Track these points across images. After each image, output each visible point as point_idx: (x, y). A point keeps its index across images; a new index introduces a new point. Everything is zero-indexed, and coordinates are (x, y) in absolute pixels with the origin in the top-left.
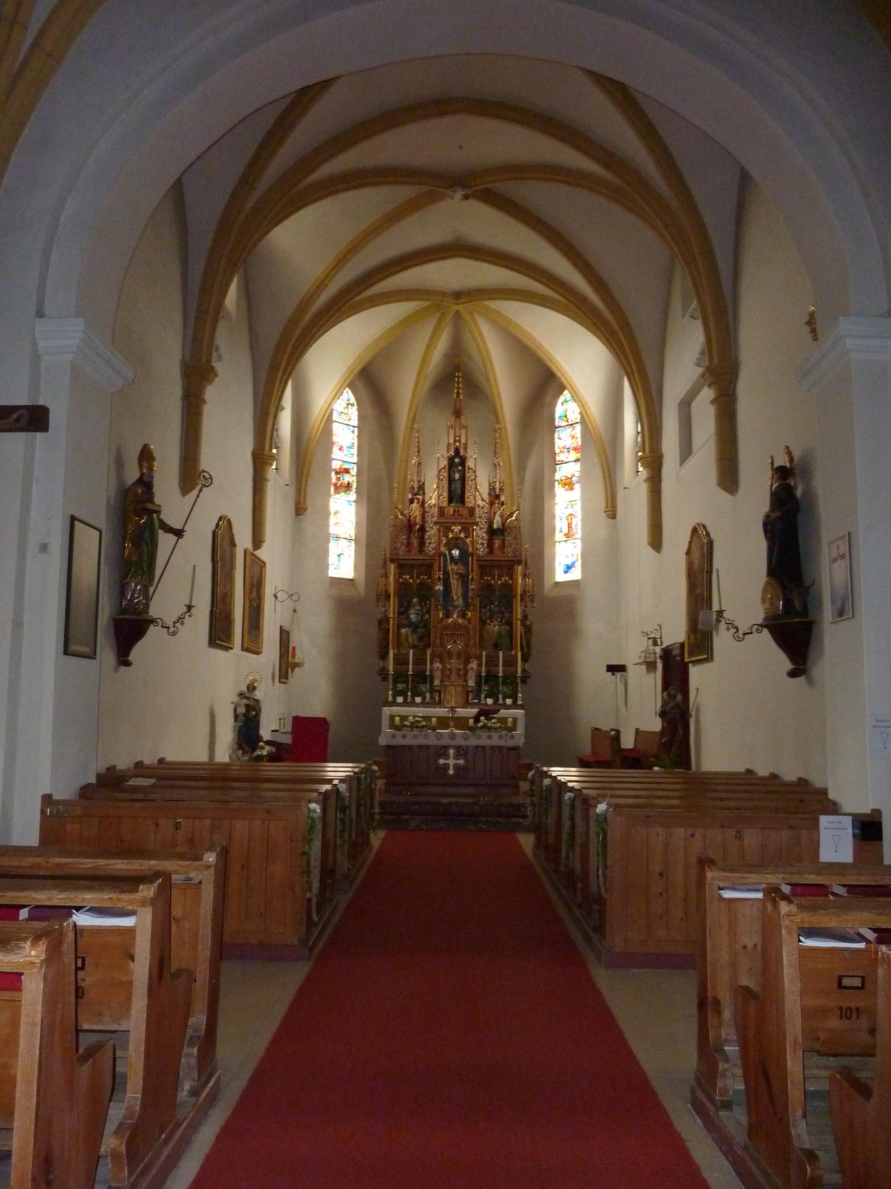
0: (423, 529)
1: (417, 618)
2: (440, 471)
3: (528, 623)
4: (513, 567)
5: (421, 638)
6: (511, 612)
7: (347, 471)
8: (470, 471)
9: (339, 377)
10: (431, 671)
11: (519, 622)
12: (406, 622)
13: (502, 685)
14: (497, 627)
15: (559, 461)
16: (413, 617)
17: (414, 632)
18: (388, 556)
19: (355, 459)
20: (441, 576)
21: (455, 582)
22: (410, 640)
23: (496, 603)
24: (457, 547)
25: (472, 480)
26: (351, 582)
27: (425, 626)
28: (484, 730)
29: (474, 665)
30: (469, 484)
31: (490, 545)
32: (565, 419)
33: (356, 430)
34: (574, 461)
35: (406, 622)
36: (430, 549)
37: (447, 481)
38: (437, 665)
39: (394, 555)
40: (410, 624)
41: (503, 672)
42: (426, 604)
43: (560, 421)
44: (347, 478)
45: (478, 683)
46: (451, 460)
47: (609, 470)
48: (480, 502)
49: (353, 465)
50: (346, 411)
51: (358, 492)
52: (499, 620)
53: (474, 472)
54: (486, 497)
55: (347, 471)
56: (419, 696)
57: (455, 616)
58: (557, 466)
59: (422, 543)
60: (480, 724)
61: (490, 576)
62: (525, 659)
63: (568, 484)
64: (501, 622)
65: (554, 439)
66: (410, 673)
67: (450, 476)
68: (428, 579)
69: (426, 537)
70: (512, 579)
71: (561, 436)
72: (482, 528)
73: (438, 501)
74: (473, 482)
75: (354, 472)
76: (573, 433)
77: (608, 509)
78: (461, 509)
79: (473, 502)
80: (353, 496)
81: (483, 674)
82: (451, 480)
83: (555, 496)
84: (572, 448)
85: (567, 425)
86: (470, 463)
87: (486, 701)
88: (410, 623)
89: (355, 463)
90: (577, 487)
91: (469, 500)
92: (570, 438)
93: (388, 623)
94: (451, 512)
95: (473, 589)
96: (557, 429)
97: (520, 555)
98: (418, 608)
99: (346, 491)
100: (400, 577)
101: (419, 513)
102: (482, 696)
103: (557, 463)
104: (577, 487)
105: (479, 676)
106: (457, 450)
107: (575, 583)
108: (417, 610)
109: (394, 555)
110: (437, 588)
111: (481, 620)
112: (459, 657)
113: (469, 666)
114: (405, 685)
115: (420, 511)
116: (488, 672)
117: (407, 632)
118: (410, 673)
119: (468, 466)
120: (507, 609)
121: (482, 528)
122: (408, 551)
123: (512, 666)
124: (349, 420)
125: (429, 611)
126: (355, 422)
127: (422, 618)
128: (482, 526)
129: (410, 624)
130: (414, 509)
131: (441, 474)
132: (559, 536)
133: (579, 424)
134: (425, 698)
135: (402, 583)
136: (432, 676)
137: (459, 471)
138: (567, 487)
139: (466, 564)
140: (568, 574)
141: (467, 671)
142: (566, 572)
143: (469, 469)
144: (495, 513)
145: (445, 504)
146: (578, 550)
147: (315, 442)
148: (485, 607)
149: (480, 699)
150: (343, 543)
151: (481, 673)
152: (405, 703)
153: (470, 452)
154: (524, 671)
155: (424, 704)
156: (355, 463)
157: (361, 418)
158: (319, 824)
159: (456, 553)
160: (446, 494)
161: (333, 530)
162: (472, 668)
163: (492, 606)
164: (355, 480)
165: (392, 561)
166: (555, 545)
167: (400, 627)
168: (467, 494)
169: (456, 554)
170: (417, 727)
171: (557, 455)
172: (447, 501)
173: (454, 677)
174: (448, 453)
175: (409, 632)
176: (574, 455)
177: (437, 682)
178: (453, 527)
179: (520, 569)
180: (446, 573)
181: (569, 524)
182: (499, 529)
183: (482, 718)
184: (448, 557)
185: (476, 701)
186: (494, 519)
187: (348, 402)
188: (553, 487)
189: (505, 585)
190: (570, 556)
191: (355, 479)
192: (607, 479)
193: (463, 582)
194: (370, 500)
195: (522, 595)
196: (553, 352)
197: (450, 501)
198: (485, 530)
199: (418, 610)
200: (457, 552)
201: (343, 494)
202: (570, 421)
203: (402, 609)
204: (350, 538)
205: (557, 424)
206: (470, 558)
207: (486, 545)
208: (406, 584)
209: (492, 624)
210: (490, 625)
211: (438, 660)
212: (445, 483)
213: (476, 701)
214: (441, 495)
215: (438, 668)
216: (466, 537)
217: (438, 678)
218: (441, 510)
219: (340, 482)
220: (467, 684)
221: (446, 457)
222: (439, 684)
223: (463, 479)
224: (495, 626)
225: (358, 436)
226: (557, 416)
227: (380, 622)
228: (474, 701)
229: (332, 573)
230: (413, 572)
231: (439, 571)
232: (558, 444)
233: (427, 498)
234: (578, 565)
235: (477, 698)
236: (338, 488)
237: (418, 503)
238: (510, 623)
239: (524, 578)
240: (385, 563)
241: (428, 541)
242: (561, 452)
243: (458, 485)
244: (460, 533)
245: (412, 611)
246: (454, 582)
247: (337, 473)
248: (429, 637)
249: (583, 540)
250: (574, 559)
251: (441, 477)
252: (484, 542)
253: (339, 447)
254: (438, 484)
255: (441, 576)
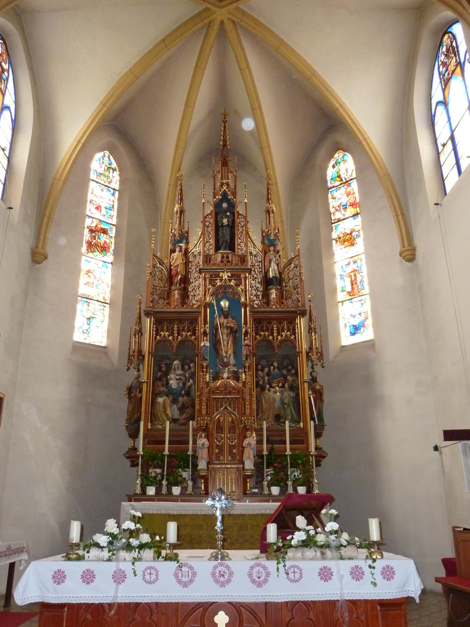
0: (185, 280)
1: (178, 384)
2: (205, 217)
3: (318, 387)
4: (295, 320)
5: (182, 409)
6: (296, 374)
7: (104, 231)
8: (240, 217)
9: (91, 113)
10: (195, 451)
11: (306, 385)
12: (163, 389)
13: (291, 467)
14: (278, 394)
15: (335, 220)
16: (173, 383)
17: (174, 401)
18: (143, 308)
19: (114, 221)
20: (208, 330)
21: (225, 337)
22: (169, 412)
23: (276, 364)
24: (225, 297)
25: (242, 227)
26: (104, 349)
27: (188, 394)
28: (310, 553)
29: (251, 440)
30: (239, 230)
31: (266, 295)
32: (338, 179)
33: (117, 194)
34: (352, 217)
35: (163, 389)
36: (194, 302)
37: (214, 227)
38: (203, 441)
39: (149, 307)
40: (170, 392)
41: (291, 450)
42: (190, 368)
43: (333, 182)
44: (103, 238)
45: (259, 466)
46: (217, 205)
47: (400, 204)
48: (252, 249)
49: (112, 226)
50: (107, 174)
51: (115, 253)
52: (280, 385)
53: (245, 217)
54: (259, 245)
55: (104, 231)
56: (177, 485)
57: (225, 375)
58: (333, 225)
59: (185, 295)
60: (299, 536)
61: (267, 330)
62: (318, 435)
63: (347, 240)
64: (283, 386)
65: (327, 199)
66: (166, 452)
67: (216, 222)
68: (191, 336)
69: (190, 290)
70: (294, 333)
71: (335, 196)
72: (256, 278)
73: (204, 249)
74: (244, 229)
75: (113, 233)
76: (349, 189)
77: (404, 249)
78: (230, 256)
79: (244, 249)
80: (109, 257)
81: (265, 453)
82: (218, 227)
83: (333, 254)
84: (348, 205)
85: (341, 184)
86: (240, 209)
87: (270, 490)
88: (169, 391)
89: (113, 225)
90: (360, 242)
91: (239, 247)
92: (345, 195)
93: (141, 391)
94: (219, 259)
95: (247, 345)
96: (330, 190)
97: (303, 305)
98: (180, 372)
99: (102, 251)
100: (157, 334)
101: (181, 261)
102: (265, 483)
103: (333, 222)
104: (360, 242)
105: (259, 455)
106: (225, 195)
107: (369, 345)
108: (177, 375)
109: (149, 307)
110: (202, 344)
111: (258, 385)
112: (232, 429)
113: (246, 442)
114: (159, 471)
115: (183, 260)
116: (271, 451)
117: (164, 401)
118: (166, 452)
119: (238, 212)
120: (289, 371)
121: (256, 278)
122: (168, 303)
123: (302, 442)
124: (109, 183)
125: (193, 376)
126: (116, 185)
127: (184, 384)
128: (255, 276)
129: (170, 392)
130: (175, 258)
131: (207, 220)
132: (341, 296)
133: (355, 180)
134: (187, 488)
135: (160, 341)
136: (195, 457)
137: (227, 217)
138: (346, 243)
139: (237, 318)
140: (356, 335)
141: (244, 448)
142: (353, 334)
143: (239, 214)
144: (270, 261)
145: (212, 252)
146: (368, 306)
147: (61, 183)
148: (262, 370)
149: (262, 488)
150: (95, 305)
151: (262, 451)
152: (159, 496)
153: (239, 197)
154: (317, 448)
155: (184, 497)
156: (113, 225)
157: (122, 182)
158: (226, 521)
159: (224, 304)
160: (212, 241)
161: (82, 290)
162: (249, 444)
163: (272, 368)
164: (113, 242)
165: (148, 314)
166: (337, 305)
167: (155, 395)
168: (237, 241)
169: (225, 305)
170: (129, 547)
171: (332, 214)
172: (213, 249)
173: (226, 457)
174: (214, 197)
175: (168, 402)
176: (351, 211)
177: (202, 465)
178: (221, 274)
179: (302, 323)
180: (215, 329)
181: (352, 282)
182: (274, 276)
183: (301, 521)
184: (216, 308)
185: (256, 490)
186: (270, 267)
187: (110, 166)
188: (331, 246)
189: (286, 340)
190: (357, 316)
191: (113, 240)
192: (400, 217)
193: (234, 338)
194: (128, 260)
195: (307, 353)
196: (328, 81)
197: (217, 248)
198: (260, 280)
199: (180, 375)
200: (227, 304)
201: (97, 253)
202: (344, 179)
203: (160, 374)
204: (103, 301)
205: (329, 185)
206: (243, 310)
207: (261, 297)
208: (164, 340)
209: (272, 390)
210: (269, 391)
211: (203, 435)
212: (211, 229)
213: (256, 490)
214: (207, 242)
215: (203, 444)
216: (237, 285)
217: (202, 458)
218: (207, 259)
219: (94, 241)
220: (243, 467)
221: (212, 203)
222: (206, 468)
223: (232, 226)
224: (275, 392)
225: (119, 200)
226: (329, 178)
227: (130, 390)
228: (253, 490)
229: (78, 337)
230: (173, 327)
231: (205, 323)
232: (333, 203)
233: (191, 246)
234: (369, 322)
235: (258, 486)
236: (91, 246)
237: (180, 251)
238: (294, 388)
239: (309, 332)
240: (140, 318)
241: (192, 294)
242: (337, 210)
243: (227, 232)
244: (230, 281)
245: (172, 376)
246: (223, 336)
247: (91, 231)
248: (194, 407)
249: (373, 296)
250: (362, 318)
251: (207, 224)
252: (259, 293)
253: (95, 206)
254: (204, 230)
255: (208, 330)
